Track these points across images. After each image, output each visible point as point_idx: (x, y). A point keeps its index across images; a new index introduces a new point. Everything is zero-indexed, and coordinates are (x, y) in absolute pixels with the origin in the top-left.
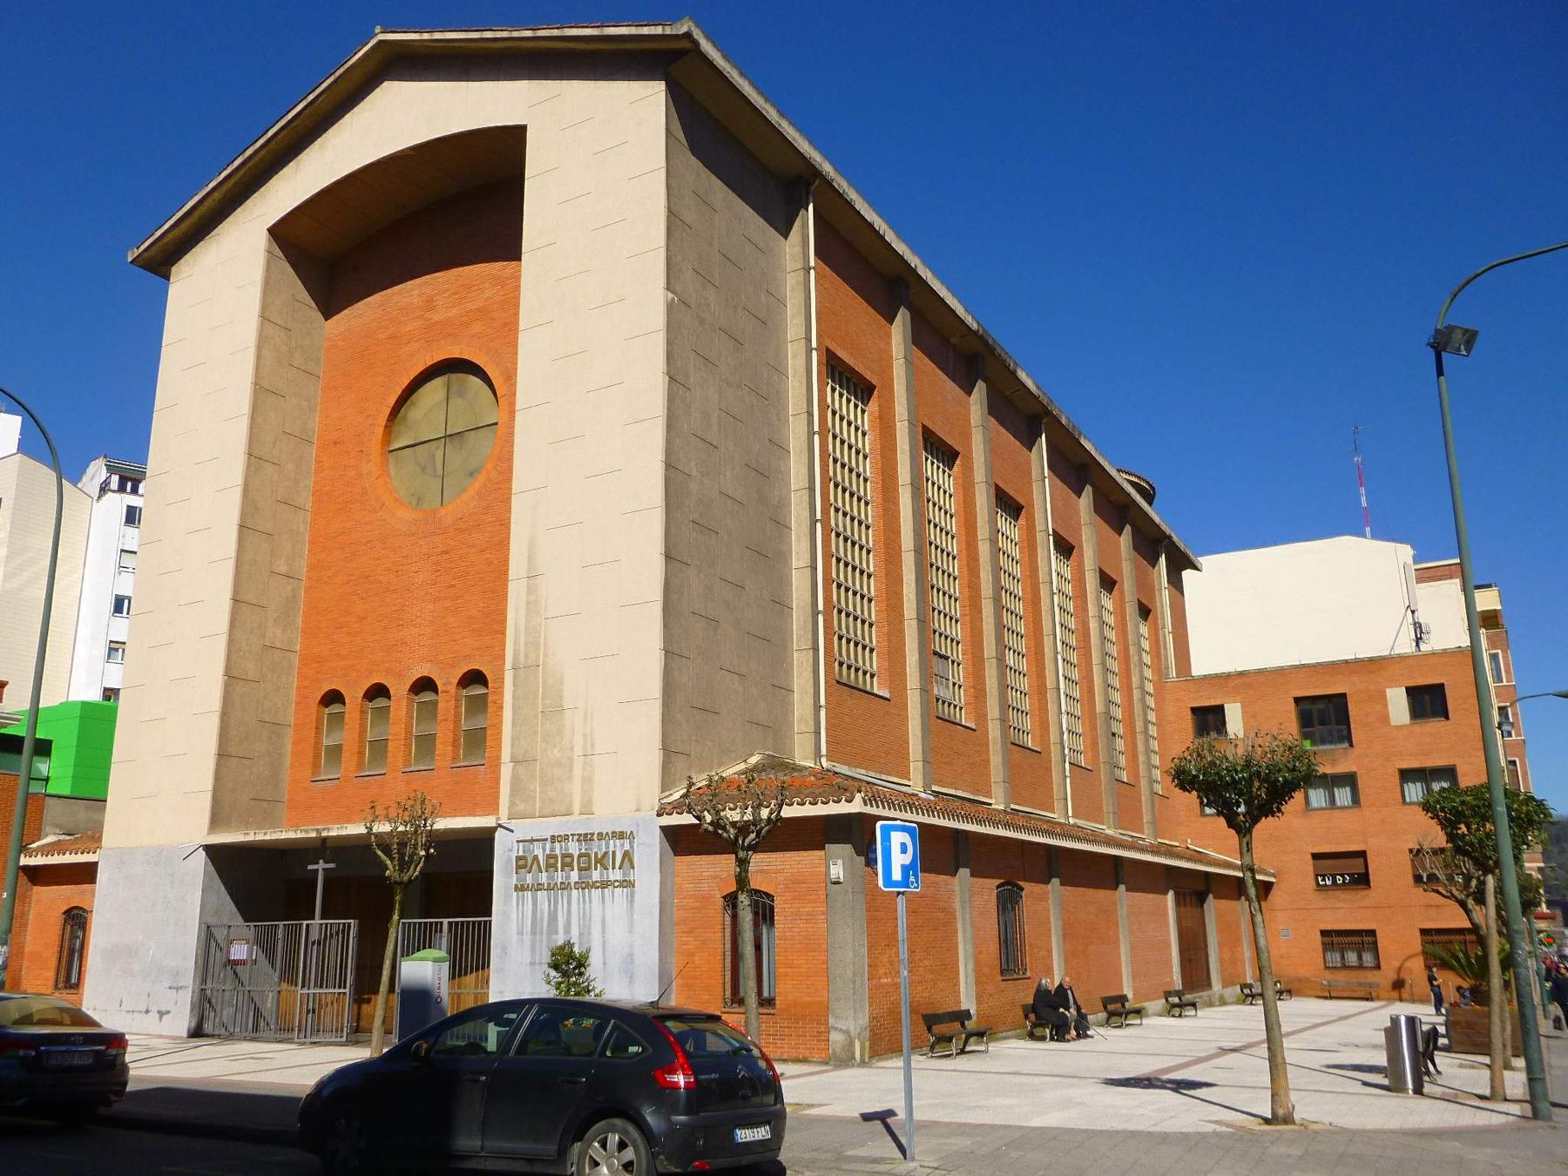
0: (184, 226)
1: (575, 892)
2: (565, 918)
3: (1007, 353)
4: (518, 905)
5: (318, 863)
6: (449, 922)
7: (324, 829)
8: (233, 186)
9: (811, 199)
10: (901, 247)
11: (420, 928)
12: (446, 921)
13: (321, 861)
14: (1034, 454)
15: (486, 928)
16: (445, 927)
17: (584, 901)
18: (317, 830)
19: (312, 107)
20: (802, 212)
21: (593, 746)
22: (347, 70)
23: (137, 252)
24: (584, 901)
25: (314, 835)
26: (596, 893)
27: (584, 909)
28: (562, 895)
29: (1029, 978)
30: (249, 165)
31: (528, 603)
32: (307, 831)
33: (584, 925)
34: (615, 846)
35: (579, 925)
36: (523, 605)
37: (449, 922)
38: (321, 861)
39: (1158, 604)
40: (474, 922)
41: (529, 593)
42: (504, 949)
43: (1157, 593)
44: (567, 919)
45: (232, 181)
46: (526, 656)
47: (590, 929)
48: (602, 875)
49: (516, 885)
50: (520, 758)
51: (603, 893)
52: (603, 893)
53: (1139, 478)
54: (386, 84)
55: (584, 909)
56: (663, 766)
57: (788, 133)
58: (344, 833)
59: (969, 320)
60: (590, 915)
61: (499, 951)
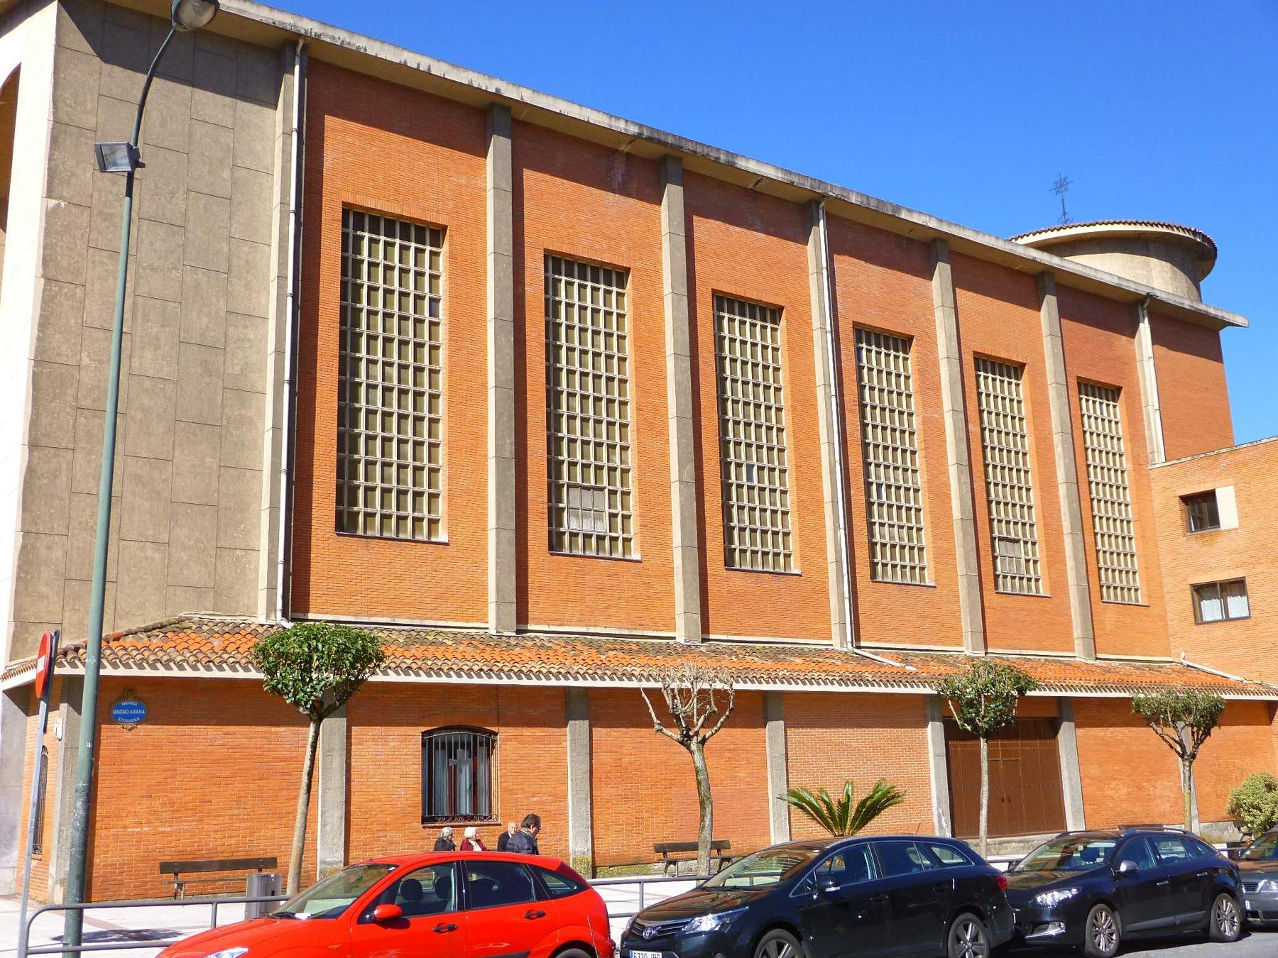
3: (718, 150)
9: (297, 60)
10: (463, 77)
14: (810, 247)
20: (287, 76)
29: (500, 825)
39: (1140, 378)
43: (1138, 364)
53: (1168, 226)
56: (14, 636)
57: (228, 7)
59: (620, 126)
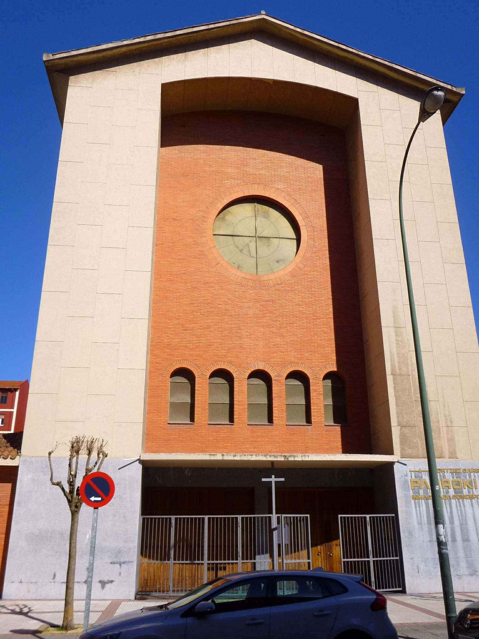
0: (92, 56)
1: (453, 501)
2: (449, 515)
4: (416, 507)
5: (271, 477)
6: (242, 517)
7: (290, 456)
8: (135, 49)
11: (380, 520)
12: (173, 517)
13: (273, 476)
15: (395, 521)
16: (173, 522)
17: (460, 506)
18: (285, 456)
19: (208, 31)
21: (451, 422)
22: (390, 66)
23: (51, 57)
24: (460, 506)
25: (282, 459)
26: (467, 502)
27: (461, 510)
28: (445, 502)
30: (154, 43)
31: (397, 341)
32: (275, 457)
33: (462, 519)
34: (475, 476)
35: (459, 519)
36: (394, 342)
37: (242, 517)
38: (273, 476)
40: (159, 519)
41: (397, 335)
42: (410, 533)
44: (450, 515)
45: (137, 46)
46: (400, 369)
47: (466, 522)
48: (469, 492)
49: (413, 496)
50: (404, 424)
51: (471, 502)
52: (471, 502)
54: (253, 41)
55: (461, 510)
58: (307, 459)
60: (465, 513)
61: (406, 534)
